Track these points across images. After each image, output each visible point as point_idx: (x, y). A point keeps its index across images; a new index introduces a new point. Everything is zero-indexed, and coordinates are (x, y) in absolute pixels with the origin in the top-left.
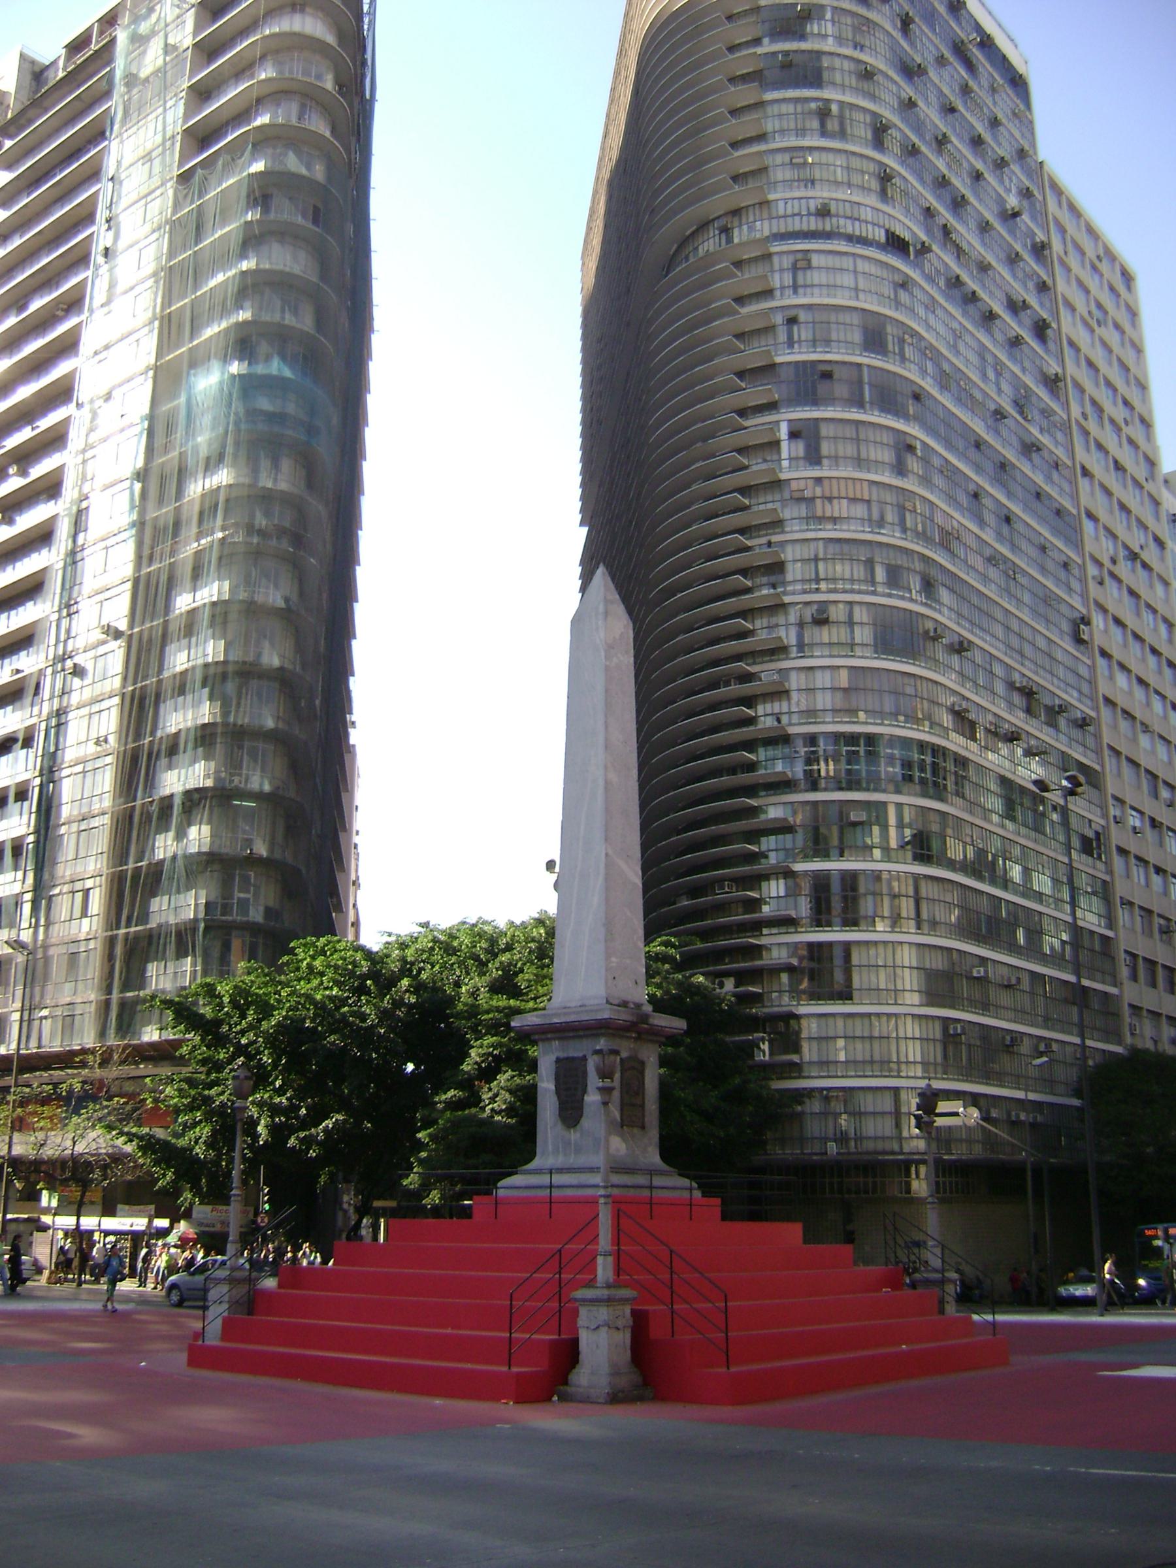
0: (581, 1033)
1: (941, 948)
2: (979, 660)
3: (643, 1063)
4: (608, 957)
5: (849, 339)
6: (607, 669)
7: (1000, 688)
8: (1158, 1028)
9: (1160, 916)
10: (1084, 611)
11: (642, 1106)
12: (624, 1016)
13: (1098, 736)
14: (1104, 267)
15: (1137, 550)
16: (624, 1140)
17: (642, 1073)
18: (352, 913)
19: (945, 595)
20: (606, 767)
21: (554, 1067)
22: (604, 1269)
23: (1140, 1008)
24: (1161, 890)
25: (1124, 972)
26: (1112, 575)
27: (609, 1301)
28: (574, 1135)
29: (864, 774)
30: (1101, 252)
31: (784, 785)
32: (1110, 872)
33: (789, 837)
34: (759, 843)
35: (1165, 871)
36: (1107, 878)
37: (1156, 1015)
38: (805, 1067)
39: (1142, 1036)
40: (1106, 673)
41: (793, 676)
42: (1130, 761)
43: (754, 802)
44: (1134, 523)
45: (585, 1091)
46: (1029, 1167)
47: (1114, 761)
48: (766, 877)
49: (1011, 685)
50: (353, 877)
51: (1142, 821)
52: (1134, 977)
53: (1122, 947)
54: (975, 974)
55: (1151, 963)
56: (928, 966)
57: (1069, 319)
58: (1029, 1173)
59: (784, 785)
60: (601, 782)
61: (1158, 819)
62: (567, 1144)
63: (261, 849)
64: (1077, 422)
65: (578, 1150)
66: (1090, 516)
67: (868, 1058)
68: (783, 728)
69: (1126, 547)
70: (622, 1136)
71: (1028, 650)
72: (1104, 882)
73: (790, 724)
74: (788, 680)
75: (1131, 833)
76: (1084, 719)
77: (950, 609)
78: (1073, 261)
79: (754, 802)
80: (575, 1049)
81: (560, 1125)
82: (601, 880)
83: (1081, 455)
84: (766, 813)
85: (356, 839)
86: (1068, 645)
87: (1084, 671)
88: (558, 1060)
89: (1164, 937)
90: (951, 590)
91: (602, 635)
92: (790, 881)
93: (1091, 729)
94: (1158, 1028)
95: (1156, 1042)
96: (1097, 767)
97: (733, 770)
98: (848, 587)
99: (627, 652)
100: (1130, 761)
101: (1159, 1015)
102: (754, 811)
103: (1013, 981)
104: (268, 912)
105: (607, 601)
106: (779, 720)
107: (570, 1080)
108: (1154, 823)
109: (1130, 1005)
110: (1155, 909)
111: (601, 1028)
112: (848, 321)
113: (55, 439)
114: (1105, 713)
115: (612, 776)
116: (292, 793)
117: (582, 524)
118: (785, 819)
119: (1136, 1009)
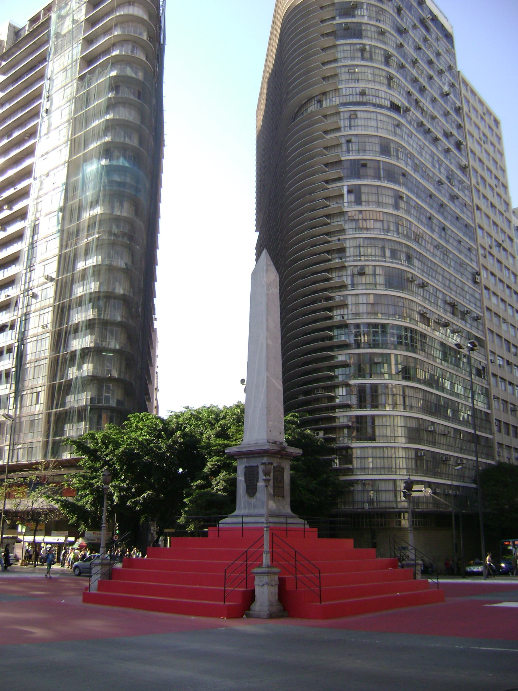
0: (256, 455)
1: (414, 418)
2: (431, 291)
3: (283, 469)
4: (268, 422)
5: (374, 149)
6: (267, 295)
7: (440, 303)
8: (510, 453)
9: (511, 403)
10: (478, 269)
11: (283, 487)
12: (275, 448)
13: (483, 324)
14: (486, 118)
15: (501, 242)
16: (275, 503)
17: (283, 473)
18: (155, 402)
19: (416, 262)
20: (267, 338)
21: (244, 470)
22: (266, 559)
23: (502, 444)
24: (511, 392)
25: (495, 428)
26: (490, 253)
27: (268, 573)
28: (253, 500)
29: (380, 341)
30: (485, 111)
31: (345, 346)
32: (489, 384)
33: (347, 369)
34: (334, 371)
35: (513, 384)
36: (488, 387)
37: (509, 447)
38: (355, 470)
39: (503, 457)
40: (487, 297)
41: (349, 298)
42: (498, 335)
43: (332, 354)
44: (499, 230)
45: (257, 481)
46: (453, 514)
47: (491, 335)
48: (337, 386)
49: (445, 302)
50: (155, 387)
51: (503, 362)
52: (500, 431)
53: (494, 417)
54: (430, 429)
55: (507, 425)
56: (409, 426)
57: (471, 140)
58: (453, 517)
59: (345, 346)
60: (265, 345)
61: (510, 361)
62: (250, 504)
63: (115, 374)
64: (474, 186)
65: (255, 507)
66: (480, 227)
67: (382, 466)
68: (345, 321)
69: (496, 241)
70: (274, 501)
71: (453, 287)
72: (486, 389)
73: (348, 319)
74: (347, 300)
75: (498, 367)
76: (477, 317)
77: (419, 268)
78: (473, 115)
79: (332, 354)
80: (253, 462)
81: (247, 496)
82: (265, 388)
83: (476, 201)
84: (338, 358)
85: (157, 370)
86: (470, 284)
87: (477, 296)
88: (246, 467)
89: (513, 413)
90: (419, 260)
91: (265, 280)
92: (348, 388)
93: (481, 321)
94: (510, 453)
95: (509, 459)
96: (483, 338)
97: (323, 339)
98: (374, 258)
99: (276, 287)
100: (498, 335)
101: (511, 447)
102: (332, 358)
103: (446, 433)
104: (118, 402)
105: (267, 265)
106: (343, 318)
107: (251, 476)
108: (508, 363)
109: (498, 443)
110: (509, 401)
111: (265, 453)
112: (374, 141)
113: (24, 194)
114: (487, 314)
115: (270, 342)
116: (128, 350)
117: (256, 231)
118: (346, 361)
119: (500, 445)
